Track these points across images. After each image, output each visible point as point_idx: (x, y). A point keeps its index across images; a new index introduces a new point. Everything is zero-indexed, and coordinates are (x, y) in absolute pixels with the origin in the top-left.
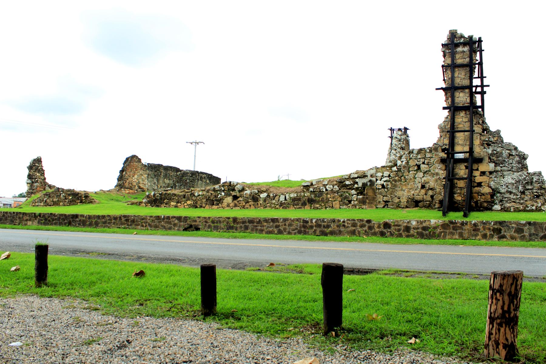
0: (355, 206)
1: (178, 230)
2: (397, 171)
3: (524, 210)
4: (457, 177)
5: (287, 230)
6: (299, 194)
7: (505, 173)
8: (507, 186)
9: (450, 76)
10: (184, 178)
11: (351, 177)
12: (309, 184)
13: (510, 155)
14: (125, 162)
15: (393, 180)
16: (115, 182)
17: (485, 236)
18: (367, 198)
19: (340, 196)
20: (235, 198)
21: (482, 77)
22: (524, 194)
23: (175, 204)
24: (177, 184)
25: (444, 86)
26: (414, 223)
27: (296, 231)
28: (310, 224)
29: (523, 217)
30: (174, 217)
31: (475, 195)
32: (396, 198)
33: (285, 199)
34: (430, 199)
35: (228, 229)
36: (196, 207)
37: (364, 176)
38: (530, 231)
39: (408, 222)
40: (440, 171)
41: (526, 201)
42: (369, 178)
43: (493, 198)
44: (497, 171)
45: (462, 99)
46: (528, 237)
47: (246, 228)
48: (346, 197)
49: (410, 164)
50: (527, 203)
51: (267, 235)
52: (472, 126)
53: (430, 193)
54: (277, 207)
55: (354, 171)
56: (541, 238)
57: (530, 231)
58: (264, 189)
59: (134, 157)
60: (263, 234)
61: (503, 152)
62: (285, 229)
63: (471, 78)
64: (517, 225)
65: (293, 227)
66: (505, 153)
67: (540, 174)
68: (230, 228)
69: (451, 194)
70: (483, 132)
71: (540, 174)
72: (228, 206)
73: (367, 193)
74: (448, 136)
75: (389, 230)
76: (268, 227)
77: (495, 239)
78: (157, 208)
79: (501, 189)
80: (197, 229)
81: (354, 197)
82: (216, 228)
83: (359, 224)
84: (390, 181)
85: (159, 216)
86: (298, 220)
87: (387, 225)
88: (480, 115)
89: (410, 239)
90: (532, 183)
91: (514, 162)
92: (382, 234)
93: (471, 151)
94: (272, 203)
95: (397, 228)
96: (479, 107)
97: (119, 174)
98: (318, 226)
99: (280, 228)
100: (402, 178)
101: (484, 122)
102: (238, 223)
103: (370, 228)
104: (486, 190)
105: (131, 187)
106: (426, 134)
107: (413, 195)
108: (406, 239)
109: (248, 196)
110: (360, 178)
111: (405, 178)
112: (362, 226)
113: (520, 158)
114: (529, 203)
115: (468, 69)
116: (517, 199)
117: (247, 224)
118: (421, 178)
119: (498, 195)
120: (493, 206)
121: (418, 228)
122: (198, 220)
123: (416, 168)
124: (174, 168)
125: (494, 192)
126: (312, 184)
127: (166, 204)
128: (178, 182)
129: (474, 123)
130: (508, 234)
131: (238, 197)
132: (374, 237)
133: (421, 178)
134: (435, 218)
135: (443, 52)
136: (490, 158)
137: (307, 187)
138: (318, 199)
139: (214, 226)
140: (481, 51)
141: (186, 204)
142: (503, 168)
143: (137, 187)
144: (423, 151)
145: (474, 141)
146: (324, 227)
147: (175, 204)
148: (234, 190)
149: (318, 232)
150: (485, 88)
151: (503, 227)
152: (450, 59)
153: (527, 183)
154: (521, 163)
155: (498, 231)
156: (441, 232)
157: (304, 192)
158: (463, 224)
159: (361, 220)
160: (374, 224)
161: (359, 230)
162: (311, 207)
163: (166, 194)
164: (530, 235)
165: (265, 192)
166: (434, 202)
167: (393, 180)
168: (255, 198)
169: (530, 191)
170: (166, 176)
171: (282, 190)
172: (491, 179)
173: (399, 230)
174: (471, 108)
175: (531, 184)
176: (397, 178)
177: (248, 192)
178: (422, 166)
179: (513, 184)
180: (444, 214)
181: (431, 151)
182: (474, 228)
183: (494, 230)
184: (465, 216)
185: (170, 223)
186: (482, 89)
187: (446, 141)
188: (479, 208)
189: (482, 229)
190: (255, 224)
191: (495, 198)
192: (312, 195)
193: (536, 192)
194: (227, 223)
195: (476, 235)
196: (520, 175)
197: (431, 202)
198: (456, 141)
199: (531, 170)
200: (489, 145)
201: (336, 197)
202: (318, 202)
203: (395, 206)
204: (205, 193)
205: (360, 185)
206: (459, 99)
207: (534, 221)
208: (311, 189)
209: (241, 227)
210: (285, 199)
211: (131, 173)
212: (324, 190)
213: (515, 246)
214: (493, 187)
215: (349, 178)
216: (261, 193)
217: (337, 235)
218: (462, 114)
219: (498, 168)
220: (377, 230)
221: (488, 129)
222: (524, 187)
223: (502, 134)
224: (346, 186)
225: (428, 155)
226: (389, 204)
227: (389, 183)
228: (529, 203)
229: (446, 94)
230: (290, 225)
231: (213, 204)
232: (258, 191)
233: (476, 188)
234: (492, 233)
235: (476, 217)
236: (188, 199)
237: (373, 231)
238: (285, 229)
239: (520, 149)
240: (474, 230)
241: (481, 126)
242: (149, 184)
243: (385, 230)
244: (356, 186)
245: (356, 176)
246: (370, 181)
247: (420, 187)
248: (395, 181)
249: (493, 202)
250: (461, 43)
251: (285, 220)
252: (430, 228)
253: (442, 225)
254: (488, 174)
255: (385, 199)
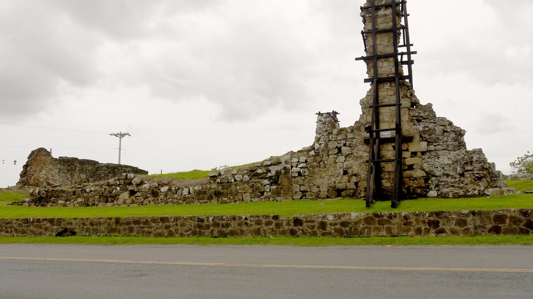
0: (268, 198)
1: (50, 235)
2: (315, 156)
3: (465, 196)
4: (384, 159)
5: (179, 232)
6: (204, 186)
7: (440, 153)
8: (443, 168)
9: (371, 44)
10: (98, 172)
11: (264, 164)
12: (216, 174)
13: (444, 131)
14: (30, 156)
15: (311, 167)
16: (18, 178)
17: (419, 231)
18: (282, 189)
19: (251, 187)
20: (132, 193)
21: (408, 45)
22: (464, 177)
23: (63, 202)
24: (90, 179)
25: (365, 55)
26: (331, 218)
27: (190, 232)
28: (206, 223)
29: (465, 206)
30: (46, 220)
31: (406, 180)
32: (315, 187)
33: (189, 193)
34: (354, 186)
35: (109, 232)
36: (88, 205)
37: (279, 163)
38: (475, 223)
39: (324, 217)
40: (363, 152)
41: (466, 184)
42: (283, 165)
43: (427, 182)
44: (430, 151)
45: (386, 69)
46: (473, 231)
47: (131, 230)
48: (258, 188)
49: (329, 146)
50: (467, 186)
51: (157, 239)
52: (399, 100)
53: (354, 179)
54: (180, 202)
55: (268, 157)
56: (490, 231)
57: (475, 223)
58: (165, 181)
59: (41, 150)
60: (150, 237)
61: (437, 128)
62: (176, 230)
63: (395, 45)
64: (459, 216)
65: (185, 228)
66: (439, 129)
67: (480, 152)
68: (112, 231)
69: (378, 180)
70: (412, 106)
71: (480, 152)
72: (124, 202)
73: (281, 182)
74: (371, 112)
75: (301, 228)
76: (157, 228)
77: (432, 234)
78: (42, 208)
79: (436, 172)
80: (74, 233)
81: (267, 188)
82: (96, 231)
83: (264, 221)
84: (306, 167)
85: (27, 219)
86: (191, 218)
87: (297, 222)
88: (408, 86)
89: (326, 238)
90: (471, 163)
91: (450, 140)
92: (293, 233)
93: (398, 128)
94: (174, 198)
95: (310, 224)
96: (406, 77)
97: (22, 169)
98: (217, 225)
99: (171, 229)
100: (321, 163)
101: (412, 95)
102: (121, 224)
103: (278, 225)
104: (418, 173)
105: (37, 184)
106: (350, 116)
107: (335, 182)
108: (322, 238)
109: (147, 190)
110: (274, 165)
111: (324, 163)
112: (268, 224)
113: (456, 134)
114: (470, 187)
115: (391, 34)
116: (456, 182)
117: (132, 225)
118: (343, 163)
119: (434, 178)
120: (427, 192)
121: (336, 224)
122: (74, 222)
123: (336, 151)
124: (92, 161)
125: (429, 176)
126: (220, 175)
127: (53, 203)
128: (91, 177)
129: (401, 96)
130: (447, 228)
131: (136, 192)
132: (283, 238)
133: (343, 163)
134: (356, 210)
135: (363, 16)
136: (421, 136)
137: (214, 177)
138: (226, 191)
139: (93, 229)
140: (406, 16)
141: (76, 202)
142: (437, 147)
143: (45, 184)
144: (343, 132)
145: (402, 117)
146: (223, 226)
147: (63, 202)
148: (130, 184)
149: (216, 233)
150: (412, 56)
151: (441, 218)
152: (371, 24)
153: (466, 163)
154: (458, 141)
155: (435, 224)
156: (365, 228)
157: (210, 183)
158: (390, 217)
159: (266, 216)
160: (282, 220)
161: (265, 228)
162: (218, 200)
163: (53, 191)
164: (475, 228)
165: (166, 185)
166: (359, 189)
167: (311, 167)
168: (155, 193)
169: (471, 172)
170: (81, 171)
171: (186, 183)
172: (424, 160)
173: (313, 227)
174: (397, 80)
175: (471, 164)
176: (315, 164)
177: (146, 186)
178: (344, 149)
179: (450, 165)
180: (368, 205)
181: (352, 131)
182: (405, 221)
183: (430, 223)
184: (394, 206)
185: (40, 227)
186: (409, 57)
187: (370, 119)
188: (412, 195)
189: (414, 223)
190: (142, 225)
191: (430, 182)
192: (219, 186)
193: (478, 174)
194: (109, 225)
195: (408, 230)
196: (458, 155)
197: (355, 190)
198: (381, 117)
199: (469, 148)
200: (419, 121)
201: (247, 189)
202: (226, 195)
203: (314, 197)
204: (97, 188)
205: (273, 173)
206: (383, 69)
207: (479, 209)
208: (218, 180)
209: (125, 229)
210: (189, 193)
211: (38, 168)
212: (233, 181)
213: (458, 243)
214: (427, 170)
215: (261, 165)
216: (162, 186)
217: (238, 235)
218: (387, 86)
219: (432, 147)
220: (286, 228)
221: (417, 103)
222: (463, 168)
223: (434, 108)
224: (257, 175)
225: (350, 136)
226: (307, 194)
227: (306, 170)
228: (470, 187)
229: (368, 65)
230: (183, 225)
231: (107, 202)
232: (159, 185)
233: (407, 172)
234: (428, 227)
235: (407, 207)
236: (79, 196)
237: (281, 229)
238: (176, 230)
239: (455, 124)
240: (404, 224)
241: (409, 99)
242: (61, 180)
243: (295, 228)
244: (269, 174)
245: (269, 163)
246: (285, 168)
247: (342, 173)
248: (313, 167)
249: (428, 187)
250: (382, 6)
251: (176, 219)
252: (350, 223)
253: (365, 219)
254: (419, 154)
255: (303, 188)
